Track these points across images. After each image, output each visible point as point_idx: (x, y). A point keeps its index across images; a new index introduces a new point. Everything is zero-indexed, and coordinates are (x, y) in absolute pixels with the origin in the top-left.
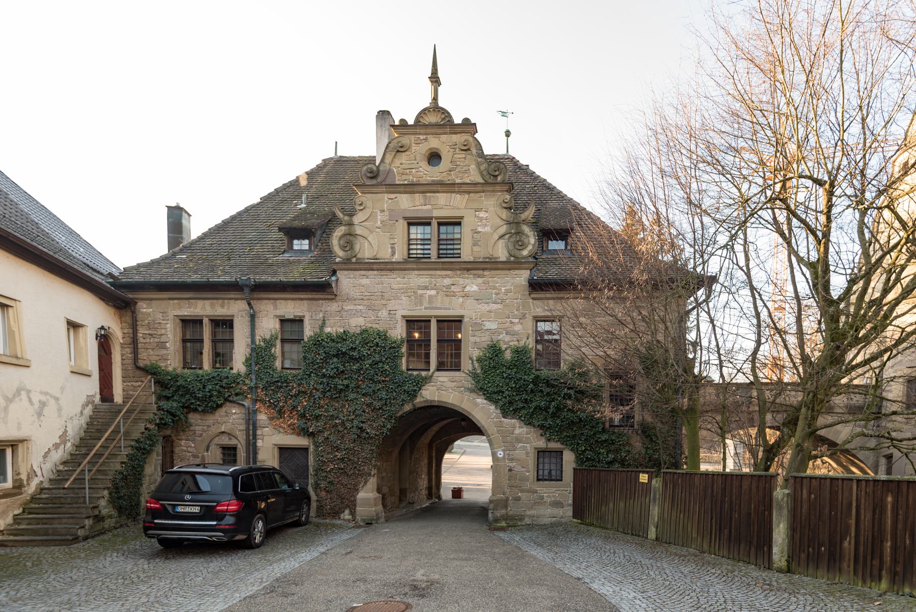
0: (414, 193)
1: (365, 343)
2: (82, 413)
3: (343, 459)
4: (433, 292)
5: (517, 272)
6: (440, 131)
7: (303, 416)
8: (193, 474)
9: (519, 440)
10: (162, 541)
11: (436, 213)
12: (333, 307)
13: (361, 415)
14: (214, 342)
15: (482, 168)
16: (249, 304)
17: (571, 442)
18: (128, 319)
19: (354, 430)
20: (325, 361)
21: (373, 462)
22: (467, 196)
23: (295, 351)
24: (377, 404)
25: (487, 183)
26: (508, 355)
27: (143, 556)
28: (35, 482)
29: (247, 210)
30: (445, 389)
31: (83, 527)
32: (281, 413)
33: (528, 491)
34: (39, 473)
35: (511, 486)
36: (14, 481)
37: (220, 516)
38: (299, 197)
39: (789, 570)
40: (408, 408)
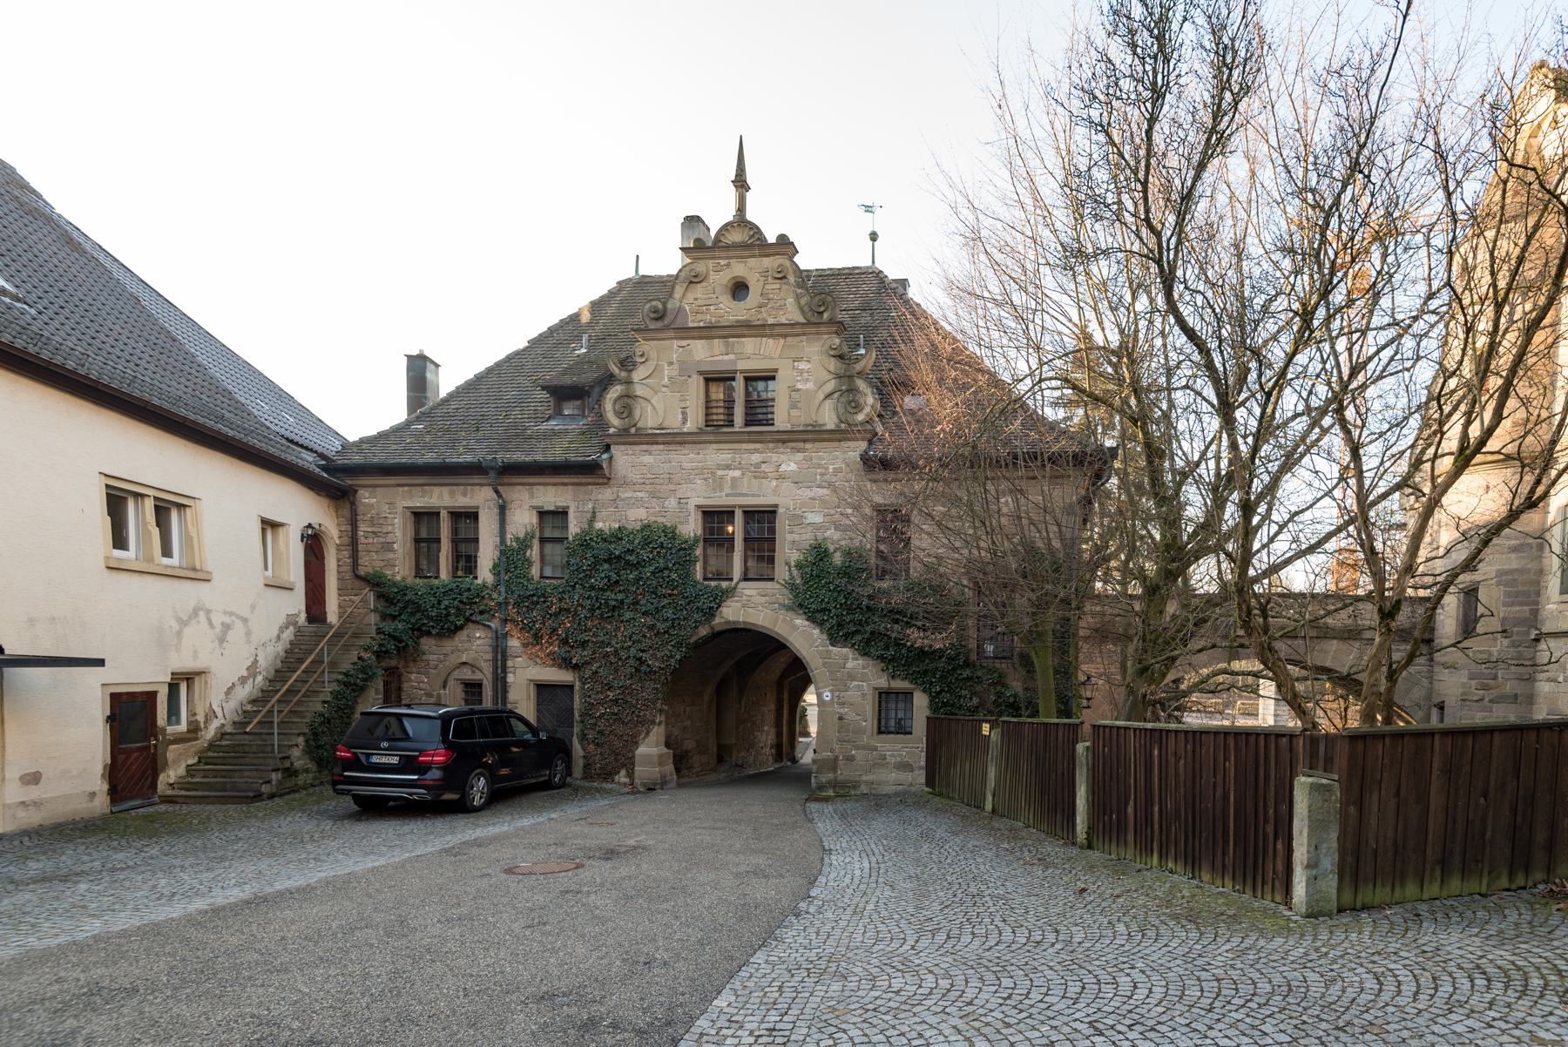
0: (713, 338)
1: (646, 542)
2: (278, 637)
3: (616, 701)
4: (737, 473)
5: (849, 444)
6: (747, 253)
7: (565, 642)
8: (399, 717)
9: (852, 677)
10: (358, 799)
11: (741, 365)
12: (606, 494)
13: (639, 641)
14: (455, 542)
15: (803, 301)
16: (497, 492)
17: (922, 678)
18: (346, 512)
19: (631, 661)
20: (594, 566)
21: (658, 705)
22: (782, 341)
23: (556, 552)
24: (661, 626)
25: (809, 323)
26: (837, 559)
27: (330, 817)
28: (214, 725)
29: (509, 359)
30: (755, 605)
31: (269, 782)
32: (537, 637)
33: (864, 748)
34: (220, 714)
35: (842, 741)
36: (189, 723)
37: (423, 769)
38: (579, 338)
39: (1090, 847)
40: (704, 631)
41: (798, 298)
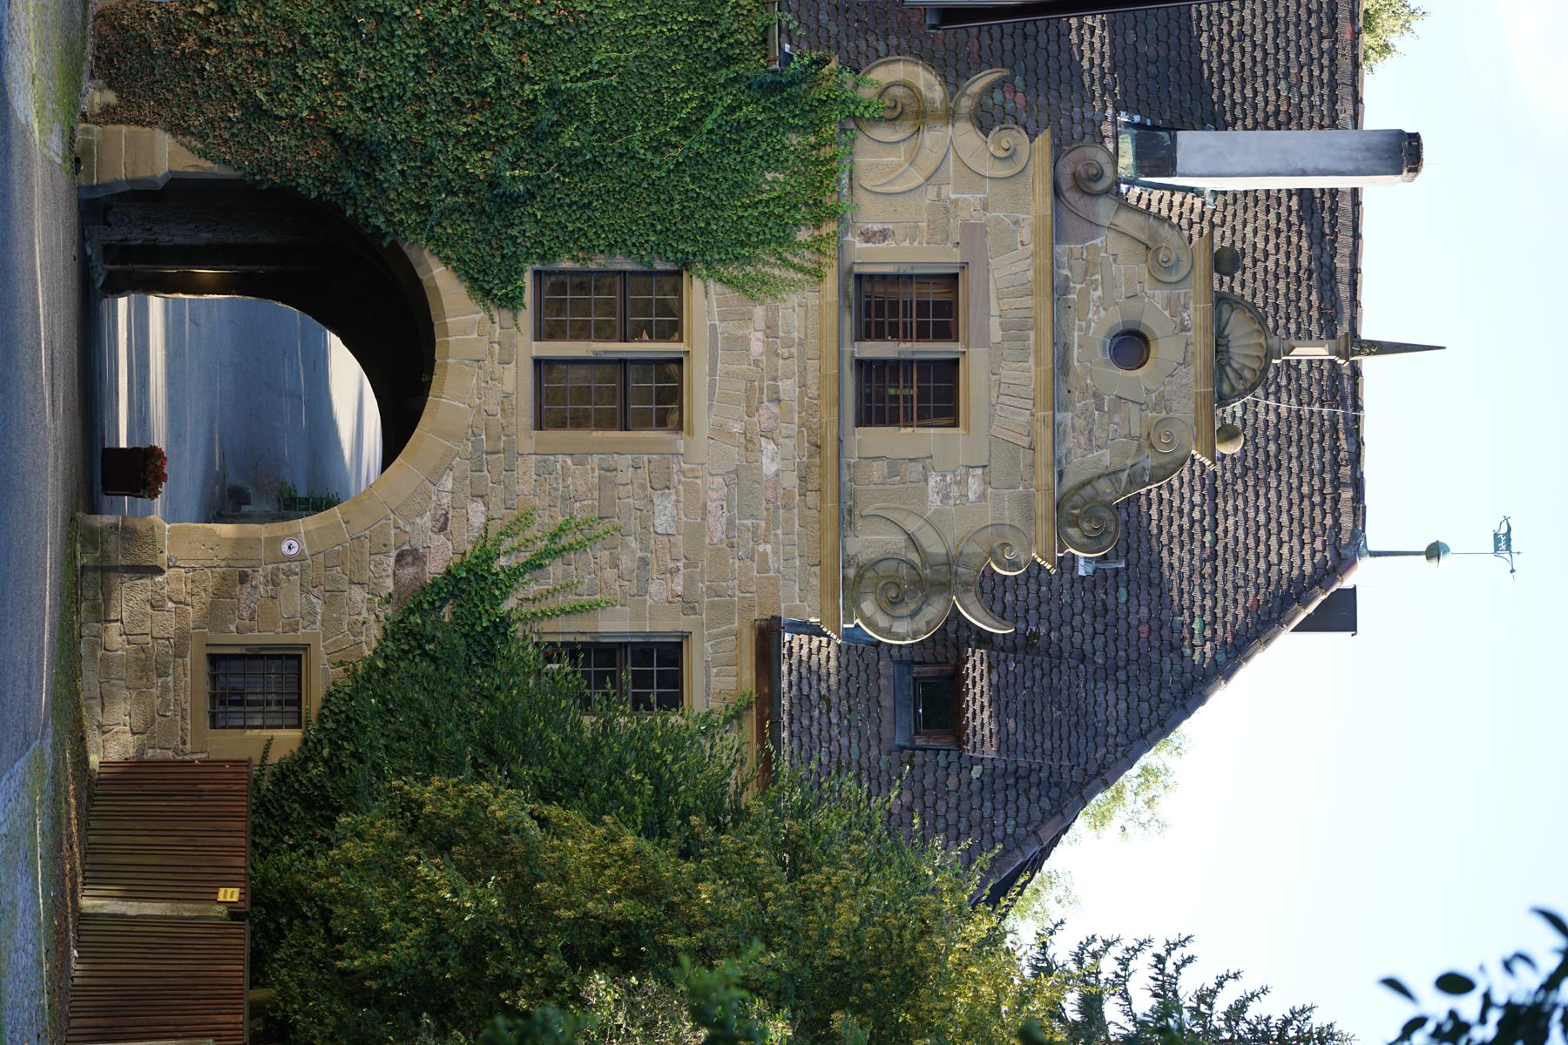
4: (757, 347)
15: (1104, 486)
41: (1112, 474)
